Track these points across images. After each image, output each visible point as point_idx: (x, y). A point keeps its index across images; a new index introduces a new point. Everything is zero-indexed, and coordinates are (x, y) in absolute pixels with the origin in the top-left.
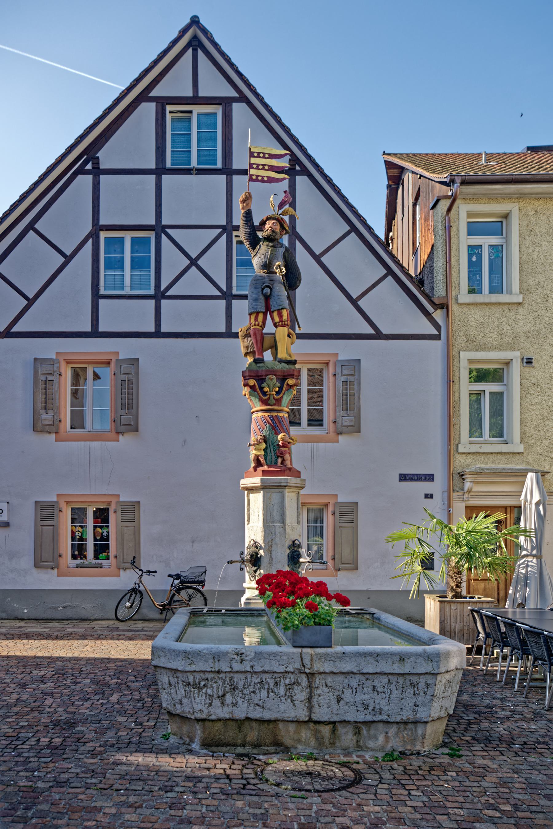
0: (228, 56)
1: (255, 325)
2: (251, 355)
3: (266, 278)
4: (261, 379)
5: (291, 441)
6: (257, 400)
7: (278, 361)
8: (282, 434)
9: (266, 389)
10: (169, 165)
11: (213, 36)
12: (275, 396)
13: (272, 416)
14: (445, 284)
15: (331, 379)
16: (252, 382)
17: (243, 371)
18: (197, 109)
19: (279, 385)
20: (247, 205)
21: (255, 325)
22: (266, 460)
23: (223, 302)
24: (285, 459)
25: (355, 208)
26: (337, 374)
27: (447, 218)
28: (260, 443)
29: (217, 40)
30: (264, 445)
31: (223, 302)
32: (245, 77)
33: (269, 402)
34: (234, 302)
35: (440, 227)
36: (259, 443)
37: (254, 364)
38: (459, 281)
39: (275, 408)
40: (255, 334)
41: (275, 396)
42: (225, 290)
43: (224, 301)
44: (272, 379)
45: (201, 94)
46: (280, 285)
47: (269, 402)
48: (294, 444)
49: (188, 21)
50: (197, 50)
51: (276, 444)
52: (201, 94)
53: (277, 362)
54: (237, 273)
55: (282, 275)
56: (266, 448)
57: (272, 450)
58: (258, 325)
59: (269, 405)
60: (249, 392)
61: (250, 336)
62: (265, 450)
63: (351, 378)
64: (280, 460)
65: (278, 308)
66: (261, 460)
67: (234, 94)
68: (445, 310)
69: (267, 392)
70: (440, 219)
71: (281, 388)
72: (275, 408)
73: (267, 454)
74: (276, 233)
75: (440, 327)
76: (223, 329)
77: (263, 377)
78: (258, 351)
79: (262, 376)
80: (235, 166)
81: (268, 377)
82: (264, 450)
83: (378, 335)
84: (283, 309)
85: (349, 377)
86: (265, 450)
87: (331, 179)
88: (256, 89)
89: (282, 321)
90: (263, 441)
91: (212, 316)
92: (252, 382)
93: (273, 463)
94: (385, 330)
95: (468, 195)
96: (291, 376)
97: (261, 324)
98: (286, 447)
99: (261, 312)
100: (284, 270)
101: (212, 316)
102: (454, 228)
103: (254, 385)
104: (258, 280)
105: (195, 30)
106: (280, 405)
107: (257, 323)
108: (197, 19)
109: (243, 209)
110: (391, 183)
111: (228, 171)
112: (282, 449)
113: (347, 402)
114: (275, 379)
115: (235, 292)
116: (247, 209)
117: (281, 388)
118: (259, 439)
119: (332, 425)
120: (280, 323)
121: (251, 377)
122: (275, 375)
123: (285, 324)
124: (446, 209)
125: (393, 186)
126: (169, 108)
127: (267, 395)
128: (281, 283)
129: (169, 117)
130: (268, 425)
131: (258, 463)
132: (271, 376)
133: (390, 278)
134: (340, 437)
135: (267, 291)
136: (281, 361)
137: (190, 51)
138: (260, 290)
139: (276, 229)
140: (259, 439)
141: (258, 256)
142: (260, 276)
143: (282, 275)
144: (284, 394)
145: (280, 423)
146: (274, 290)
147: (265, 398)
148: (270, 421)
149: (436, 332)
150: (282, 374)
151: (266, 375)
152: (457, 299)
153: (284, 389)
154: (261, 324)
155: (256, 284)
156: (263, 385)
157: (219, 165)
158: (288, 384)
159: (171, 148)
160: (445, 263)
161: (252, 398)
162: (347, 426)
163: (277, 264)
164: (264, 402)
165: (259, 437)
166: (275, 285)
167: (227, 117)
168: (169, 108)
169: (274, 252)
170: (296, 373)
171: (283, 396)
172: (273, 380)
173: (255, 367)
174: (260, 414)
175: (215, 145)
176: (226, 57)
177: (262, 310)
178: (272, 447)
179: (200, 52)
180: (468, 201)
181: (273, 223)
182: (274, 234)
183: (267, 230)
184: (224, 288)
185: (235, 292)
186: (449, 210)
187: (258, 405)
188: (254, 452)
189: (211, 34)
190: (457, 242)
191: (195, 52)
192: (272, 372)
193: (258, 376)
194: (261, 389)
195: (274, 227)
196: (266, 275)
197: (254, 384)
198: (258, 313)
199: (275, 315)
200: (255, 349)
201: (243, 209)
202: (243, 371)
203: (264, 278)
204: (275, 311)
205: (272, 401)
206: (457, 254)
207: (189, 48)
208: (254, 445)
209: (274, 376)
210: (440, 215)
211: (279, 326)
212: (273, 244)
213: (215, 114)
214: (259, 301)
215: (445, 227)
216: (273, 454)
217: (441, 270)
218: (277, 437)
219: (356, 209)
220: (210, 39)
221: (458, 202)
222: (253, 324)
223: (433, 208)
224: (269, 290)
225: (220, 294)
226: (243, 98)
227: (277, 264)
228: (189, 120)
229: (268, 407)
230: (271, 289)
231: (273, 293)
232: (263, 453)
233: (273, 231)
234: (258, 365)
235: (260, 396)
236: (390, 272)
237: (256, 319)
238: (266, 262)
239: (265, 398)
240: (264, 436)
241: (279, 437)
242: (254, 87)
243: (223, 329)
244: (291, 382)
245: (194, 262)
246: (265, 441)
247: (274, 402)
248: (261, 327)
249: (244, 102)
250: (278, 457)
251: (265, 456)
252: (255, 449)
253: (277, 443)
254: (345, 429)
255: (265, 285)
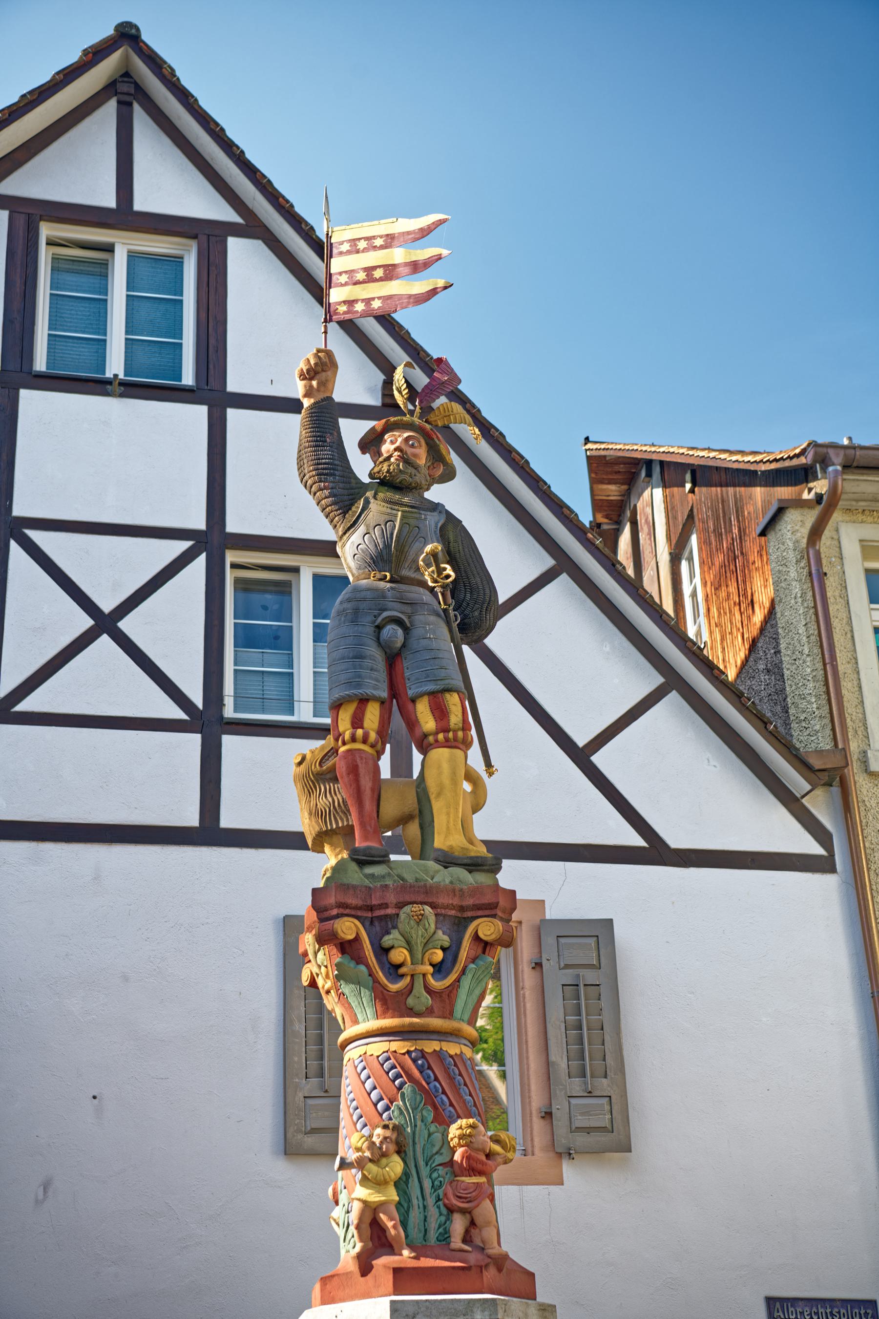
0: (217, 124)
1: (353, 739)
2: (339, 840)
3: (389, 594)
4: (379, 920)
5: (497, 1148)
6: (366, 994)
7: (437, 861)
8: (463, 1122)
9: (399, 955)
10: (40, 364)
11: (178, 73)
12: (431, 980)
13: (423, 1054)
14: (827, 721)
15: (529, 977)
16: (348, 928)
17: (315, 891)
18: (124, 245)
19: (444, 938)
20: (323, 384)
21: (353, 739)
22: (404, 1224)
23: (193, 741)
24: (479, 1221)
25: (569, 508)
26: (544, 962)
27: (811, 552)
28: (384, 1155)
29: (186, 82)
30: (395, 1166)
31: (193, 741)
32: (264, 176)
33: (410, 1001)
34: (229, 742)
35: (793, 574)
36: (379, 1156)
37: (354, 866)
38: (864, 713)
39: (435, 1022)
40: (354, 770)
41: (431, 980)
42: (200, 706)
43: (197, 738)
44: (420, 919)
45: (139, 205)
46: (432, 618)
47: (410, 1001)
48: (506, 1162)
49: (110, 31)
50: (130, 104)
51: (439, 1159)
52: (139, 205)
53: (431, 864)
54: (236, 664)
55: (444, 587)
56: (406, 1174)
57: (427, 1184)
58: (365, 741)
59: (411, 1012)
60: (338, 966)
61: (335, 780)
62: (401, 1184)
63: (590, 976)
64: (458, 1225)
65: (431, 687)
66: (390, 1224)
67: (225, 213)
68: (836, 790)
69: (400, 966)
70: (792, 556)
71: (451, 952)
72: (435, 1022)
73: (409, 1201)
74: (416, 467)
75: (829, 836)
76: (191, 818)
77: (389, 911)
78: (363, 824)
79: (385, 906)
80: (233, 385)
81: (407, 909)
82: (396, 1185)
83: (656, 852)
84: (449, 690)
85: (582, 972)
86: (401, 1184)
87: (501, 434)
88: (292, 206)
89: (446, 730)
90: (392, 1147)
91: (160, 777)
92: (348, 928)
93: (433, 1236)
94: (676, 840)
95: (857, 501)
96: (489, 909)
97: (373, 736)
98: (480, 1173)
99: (375, 699)
100: (449, 571)
101: (160, 777)
102: (831, 579)
103: (357, 939)
104: (364, 600)
105: (126, 59)
106: (449, 1014)
107: (360, 732)
108: (133, 31)
109: (307, 395)
110: (600, 519)
111: (213, 393)
112: (468, 1180)
113: (582, 1051)
114: (432, 919)
115: (229, 712)
116: (321, 396)
117: (451, 952)
118: (376, 1140)
119: (538, 1125)
120: (441, 736)
121: (346, 910)
122: (433, 906)
123: (455, 739)
124: (805, 531)
125: (605, 527)
126: (46, 230)
127: (403, 976)
128: (438, 615)
129: (44, 256)
130: (407, 1088)
131: (375, 1237)
132: (416, 908)
133: (674, 696)
134: (567, 1169)
135: (393, 634)
136: (447, 860)
137: (111, 107)
138: (370, 629)
139: (415, 455)
140: (376, 1140)
141: (362, 529)
142: (368, 589)
143: (444, 587)
144: (463, 972)
145: (451, 1079)
146: (416, 632)
147: (394, 987)
148: (416, 1073)
149: (818, 850)
150: (456, 901)
151: (400, 906)
152: (864, 761)
153: (463, 955)
154: (373, 736)
155: (356, 611)
156: (387, 941)
157: (188, 379)
158: (476, 938)
159: (50, 329)
160: (819, 666)
161: (346, 989)
162: (588, 1130)
163: (428, 548)
164: (386, 1003)
165: (379, 1131)
166: (419, 618)
167: (212, 268)
168: (46, 230)
169: (413, 522)
170: (503, 903)
171: (458, 980)
172: (422, 925)
173: (355, 876)
174: (378, 1047)
175: (178, 332)
176: (212, 126)
177: (376, 693)
178: (425, 1171)
179: (139, 115)
180: (860, 517)
181: (407, 440)
182: (411, 470)
183: (388, 458)
184: (198, 699)
185: (229, 712)
186: (816, 533)
187: (370, 1011)
188: (362, 1192)
189: (173, 70)
190: (843, 615)
191: (125, 108)
192: (424, 893)
193: (371, 908)
194: (383, 952)
195: (410, 451)
196: (389, 585)
197: (357, 939)
198: (363, 701)
199: (423, 709)
200: (354, 820)
201: (307, 395)
202: (315, 891)
203: (381, 595)
204: (421, 695)
205: (421, 999)
206: (850, 645)
207: (109, 98)
208: (360, 1164)
209: (428, 909)
210: (791, 545)
211: (437, 744)
212: (406, 500)
213: (177, 262)
214: (367, 663)
215: (810, 574)
216: (430, 1201)
217: (811, 685)
218: (445, 1134)
219: (572, 511)
220: (170, 81)
221: (837, 516)
222: (347, 736)
223: (763, 533)
224: (400, 632)
225: (183, 716)
226: (253, 228)
227: (428, 548)
228: (103, 271)
229: (407, 1020)
230: (406, 630)
231: (413, 643)
232: (393, 1195)
233: (405, 459)
234: (369, 870)
235: (376, 981)
236: (673, 682)
237: (357, 722)
238: (387, 546)
239: (394, 987)
240: (396, 1128)
241: (454, 1131)
242: (287, 201)
243: (191, 818)
244: (488, 929)
245: (106, 623)
246: (400, 1151)
247: (427, 1000)
248: (372, 746)
249: (258, 238)
250: (451, 1210)
251: (403, 1208)
252: (365, 1181)
253: (444, 1159)
254: (581, 1140)
255: (385, 614)
